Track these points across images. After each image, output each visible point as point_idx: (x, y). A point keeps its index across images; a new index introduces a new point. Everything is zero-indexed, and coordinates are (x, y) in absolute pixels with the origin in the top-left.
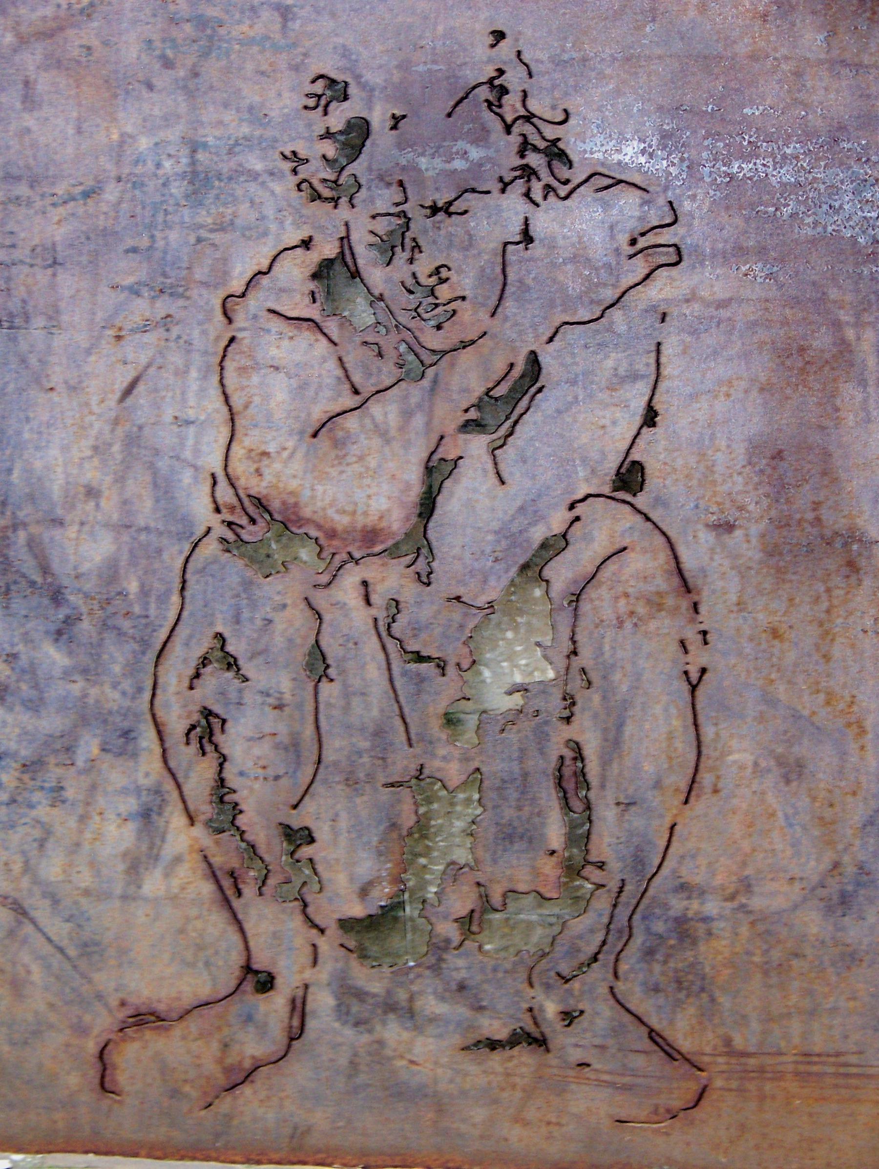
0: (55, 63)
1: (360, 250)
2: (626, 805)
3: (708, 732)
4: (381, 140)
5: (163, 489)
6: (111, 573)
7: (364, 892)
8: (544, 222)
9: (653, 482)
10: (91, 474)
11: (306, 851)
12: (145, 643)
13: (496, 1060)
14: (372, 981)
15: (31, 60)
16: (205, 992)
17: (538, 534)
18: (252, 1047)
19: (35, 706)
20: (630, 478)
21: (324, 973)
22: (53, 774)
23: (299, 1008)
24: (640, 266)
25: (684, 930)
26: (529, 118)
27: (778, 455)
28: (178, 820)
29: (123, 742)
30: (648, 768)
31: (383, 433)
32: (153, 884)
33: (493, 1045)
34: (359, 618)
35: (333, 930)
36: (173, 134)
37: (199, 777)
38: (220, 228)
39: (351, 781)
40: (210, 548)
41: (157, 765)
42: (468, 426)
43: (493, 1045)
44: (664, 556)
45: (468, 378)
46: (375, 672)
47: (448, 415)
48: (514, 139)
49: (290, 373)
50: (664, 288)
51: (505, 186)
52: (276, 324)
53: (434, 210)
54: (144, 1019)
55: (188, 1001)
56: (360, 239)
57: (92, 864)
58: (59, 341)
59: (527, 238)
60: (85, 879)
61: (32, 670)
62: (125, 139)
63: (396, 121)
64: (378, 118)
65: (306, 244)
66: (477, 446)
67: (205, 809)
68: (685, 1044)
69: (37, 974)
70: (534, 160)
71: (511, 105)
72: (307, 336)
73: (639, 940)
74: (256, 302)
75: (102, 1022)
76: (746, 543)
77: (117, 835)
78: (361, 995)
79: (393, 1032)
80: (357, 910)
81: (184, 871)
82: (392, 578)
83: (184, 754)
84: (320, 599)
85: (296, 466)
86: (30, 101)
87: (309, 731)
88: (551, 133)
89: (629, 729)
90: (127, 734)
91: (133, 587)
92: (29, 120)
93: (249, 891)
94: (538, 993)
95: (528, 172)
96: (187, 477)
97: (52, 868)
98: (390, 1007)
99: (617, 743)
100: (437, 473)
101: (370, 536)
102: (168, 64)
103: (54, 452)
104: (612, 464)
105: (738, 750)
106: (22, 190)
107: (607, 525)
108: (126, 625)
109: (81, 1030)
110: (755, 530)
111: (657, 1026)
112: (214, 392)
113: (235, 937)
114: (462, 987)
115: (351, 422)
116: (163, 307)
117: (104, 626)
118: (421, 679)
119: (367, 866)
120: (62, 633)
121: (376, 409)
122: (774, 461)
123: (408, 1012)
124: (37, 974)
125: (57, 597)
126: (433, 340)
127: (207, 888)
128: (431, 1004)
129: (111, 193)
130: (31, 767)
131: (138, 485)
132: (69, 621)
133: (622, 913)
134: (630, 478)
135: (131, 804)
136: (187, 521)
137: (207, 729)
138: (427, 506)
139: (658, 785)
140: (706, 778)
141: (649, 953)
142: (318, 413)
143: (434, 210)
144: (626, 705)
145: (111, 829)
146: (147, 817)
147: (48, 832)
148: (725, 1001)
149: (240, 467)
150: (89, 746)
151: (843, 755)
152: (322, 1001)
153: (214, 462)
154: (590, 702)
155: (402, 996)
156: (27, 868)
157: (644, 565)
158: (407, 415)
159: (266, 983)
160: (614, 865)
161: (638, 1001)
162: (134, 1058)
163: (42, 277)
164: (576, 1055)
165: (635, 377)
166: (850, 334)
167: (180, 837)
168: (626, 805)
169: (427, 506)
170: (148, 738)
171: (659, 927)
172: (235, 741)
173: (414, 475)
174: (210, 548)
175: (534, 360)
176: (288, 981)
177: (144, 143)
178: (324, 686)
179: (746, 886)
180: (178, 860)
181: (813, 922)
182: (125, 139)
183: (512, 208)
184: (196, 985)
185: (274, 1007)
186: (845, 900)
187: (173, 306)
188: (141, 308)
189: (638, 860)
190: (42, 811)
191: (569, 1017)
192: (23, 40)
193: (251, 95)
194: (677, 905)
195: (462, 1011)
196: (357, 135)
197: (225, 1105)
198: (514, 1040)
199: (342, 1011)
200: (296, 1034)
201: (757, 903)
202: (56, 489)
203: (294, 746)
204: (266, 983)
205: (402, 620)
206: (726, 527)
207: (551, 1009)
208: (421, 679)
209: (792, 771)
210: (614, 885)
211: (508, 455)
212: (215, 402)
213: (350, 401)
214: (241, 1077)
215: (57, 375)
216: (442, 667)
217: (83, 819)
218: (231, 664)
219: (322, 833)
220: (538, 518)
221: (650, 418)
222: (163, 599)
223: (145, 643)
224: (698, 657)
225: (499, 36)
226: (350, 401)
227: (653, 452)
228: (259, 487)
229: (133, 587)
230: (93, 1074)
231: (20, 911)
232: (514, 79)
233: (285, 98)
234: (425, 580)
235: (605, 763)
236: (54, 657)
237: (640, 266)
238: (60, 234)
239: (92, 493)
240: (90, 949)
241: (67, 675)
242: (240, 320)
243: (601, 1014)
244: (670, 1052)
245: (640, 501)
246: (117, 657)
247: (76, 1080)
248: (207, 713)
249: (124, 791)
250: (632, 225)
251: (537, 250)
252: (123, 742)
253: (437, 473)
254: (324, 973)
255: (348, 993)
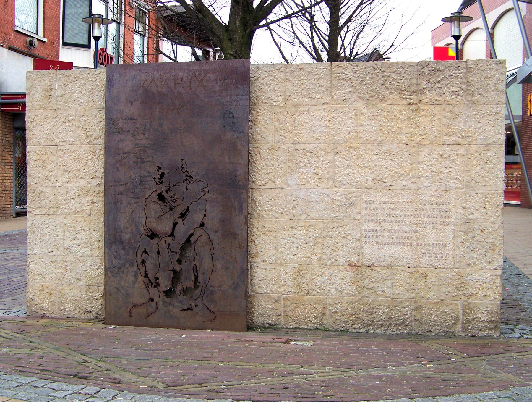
0: (121, 165)
1: (164, 192)
2: (203, 274)
3: (215, 263)
4: (166, 175)
5: (137, 227)
6: (130, 240)
7: (166, 287)
8: (189, 187)
9: (205, 225)
10: (127, 225)
11: (158, 281)
12: (135, 250)
13: (185, 312)
14: (168, 300)
15: (118, 165)
16: (144, 302)
17: (189, 233)
18: (151, 310)
19: (120, 259)
20: (202, 225)
21: (161, 299)
22: (122, 269)
23: (157, 304)
24: (203, 193)
25: (212, 293)
26: (187, 172)
27: (223, 221)
28: (140, 276)
29: (132, 265)
30: (206, 268)
31: (167, 218)
32: (137, 285)
33: (185, 310)
34: (165, 245)
35: (162, 293)
36: (137, 175)
37: (143, 270)
38: (144, 189)
39: (164, 270)
40: (144, 235)
41: (137, 267)
42: (179, 218)
43: (185, 310)
44: (207, 236)
45: (180, 210)
46: (167, 254)
47: (177, 215)
48: (185, 175)
49: (155, 208)
50: (207, 196)
51: (184, 182)
52: (152, 203)
53: (174, 185)
54: (136, 306)
55: (142, 303)
56: (164, 190)
57: (128, 283)
58: (122, 205)
59: (187, 189)
60: (127, 285)
61: (119, 254)
62: (131, 176)
63: (168, 172)
64: (166, 172)
65: (156, 191)
66: (181, 220)
67: (144, 275)
68: (212, 309)
69: (121, 299)
70: (188, 178)
71: (184, 170)
72: (156, 205)
73: (205, 294)
74: (149, 199)
75: (130, 306)
76: (220, 233)
77: (131, 279)
78: (166, 302)
79: (171, 308)
80: (165, 290)
81: (141, 283)
82: (169, 240)
83: (140, 266)
84: (159, 243)
85: (155, 223)
86: (118, 171)
87: (158, 262)
88: (190, 174)
89: (203, 262)
90: (133, 263)
91: (133, 241)
92: (118, 173)
93: (150, 286)
94: (191, 302)
95: (187, 180)
96: (140, 225)
97: (122, 283)
98: (170, 304)
99: (201, 265)
100: (175, 224)
101: (166, 234)
102: (137, 165)
103: (122, 222)
104: (199, 223)
105: (219, 265)
106: (117, 183)
107: (199, 232)
108: (132, 247)
109: (127, 307)
110: (220, 232)
111: (251, 335)
112: (144, 213)
113: (148, 293)
114: (180, 301)
115: (163, 217)
116: (136, 200)
117: (129, 247)
118: (173, 255)
119: (166, 283)
120: (123, 248)
121: (166, 215)
122: (223, 222)
123: (173, 305)
124: (121, 299)
125: (122, 243)
126: (174, 204)
127: (144, 286)
128: (176, 304)
129: (129, 184)
130: (119, 268)
131: (133, 227)
132: (124, 247)
133: (203, 291)
134: (202, 225)
135: (133, 274)
136: (141, 232)
137: (143, 262)
138: (174, 229)
139: (207, 271)
140: (214, 270)
141: (207, 296)
142: (158, 216)
143: (174, 185)
144: (202, 259)
145: (131, 277)
146: (136, 276)
147: (122, 278)
148: (218, 303)
149: (147, 224)
150: (127, 265)
151: (234, 266)
152: (161, 303)
153: (144, 223)
154: (197, 258)
155: (172, 302)
156: (119, 283)
157: (204, 238)
158: (170, 216)
159: (152, 300)
160: (201, 283)
161: (205, 303)
162: (135, 311)
163: (120, 196)
164: (197, 311)
165: (203, 210)
166: (233, 203)
167: (141, 279)
168: (203, 274)
169: (174, 229)
170: (135, 264)
171: (208, 292)
172: (147, 264)
173: (172, 225)
174: (144, 235)
175: (188, 207)
176: (156, 300)
177: (133, 176)
178: (160, 256)
179: (221, 286)
180: (140, 282)
181: (231, 291)
182: (131, 176)
183: (184, 185)
184: (143, 301)
185: (154, 304)
186: (235, 288)
187: (138, 200)
188: (133, 201)
189: (205, 282)
190: (121, 275)
191: (196, 306)
192: (117, 162)
193: (148, 169)
194: (211, 289)
195: (180, 305)
196: (162, 175)
197: (147, 319)
198: (189, 309)
199: (163, 305)
200: (157, 308)
201: (222, 289)
202: (122, 227)
203: (156, 265)
204: (152, 300)
205: (170, 246)
206: (216, 232)
207: (193, 304)
208: (173, 255)
209: (227, 268)
210: (201, 286)
211: (184, 222)
212: (144, 214)
213: (162, 214)
214: (149, 315)
215: (122, 210)
216: (176, 253)
217: (127, 276)
218: (146, 252)
219: (160, 278)
220: (189, 231)
221: (205, 216)
222: (137, 244)
223: (135, 250)
224: (213, 251)
225: (182, 160)
226: (162, 214)
227: (206, 221)
228: (150, 227)
229: (133, 241)
230: (129, 314)
231: (118, 290)
232: (185, 166)
233: (153, 169)
234: (174, 240)
235: (200, 267)
236: (122, 252)
237: (203, 193)
238: (122, 190)
239: (127, 228)
240: (128, 295)
241: (124, 255)
242: (147, 202)
243: (200, 305)
244: (211, 311)
245: (204, 228)
246: (131, 252)
247: (126, 315)
248: (143, 260)
249: (78, 134)
250: (202, 187)
251: (188, 191)
252: (132, 265)
253: (175, 224)
254: (161, 299)
255: (164, 302)
